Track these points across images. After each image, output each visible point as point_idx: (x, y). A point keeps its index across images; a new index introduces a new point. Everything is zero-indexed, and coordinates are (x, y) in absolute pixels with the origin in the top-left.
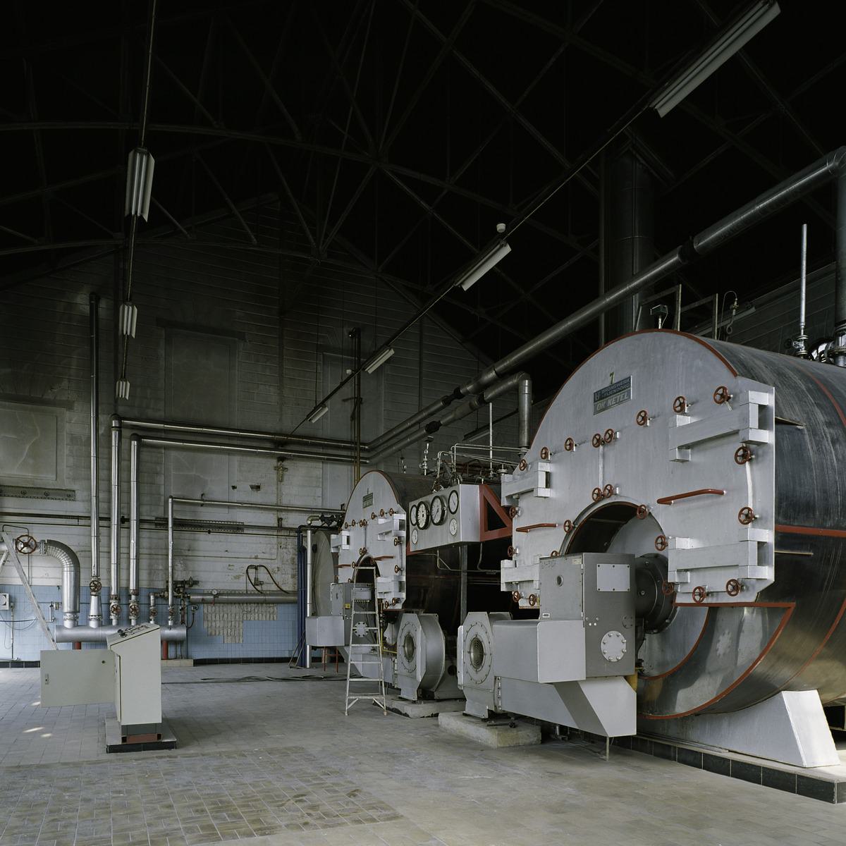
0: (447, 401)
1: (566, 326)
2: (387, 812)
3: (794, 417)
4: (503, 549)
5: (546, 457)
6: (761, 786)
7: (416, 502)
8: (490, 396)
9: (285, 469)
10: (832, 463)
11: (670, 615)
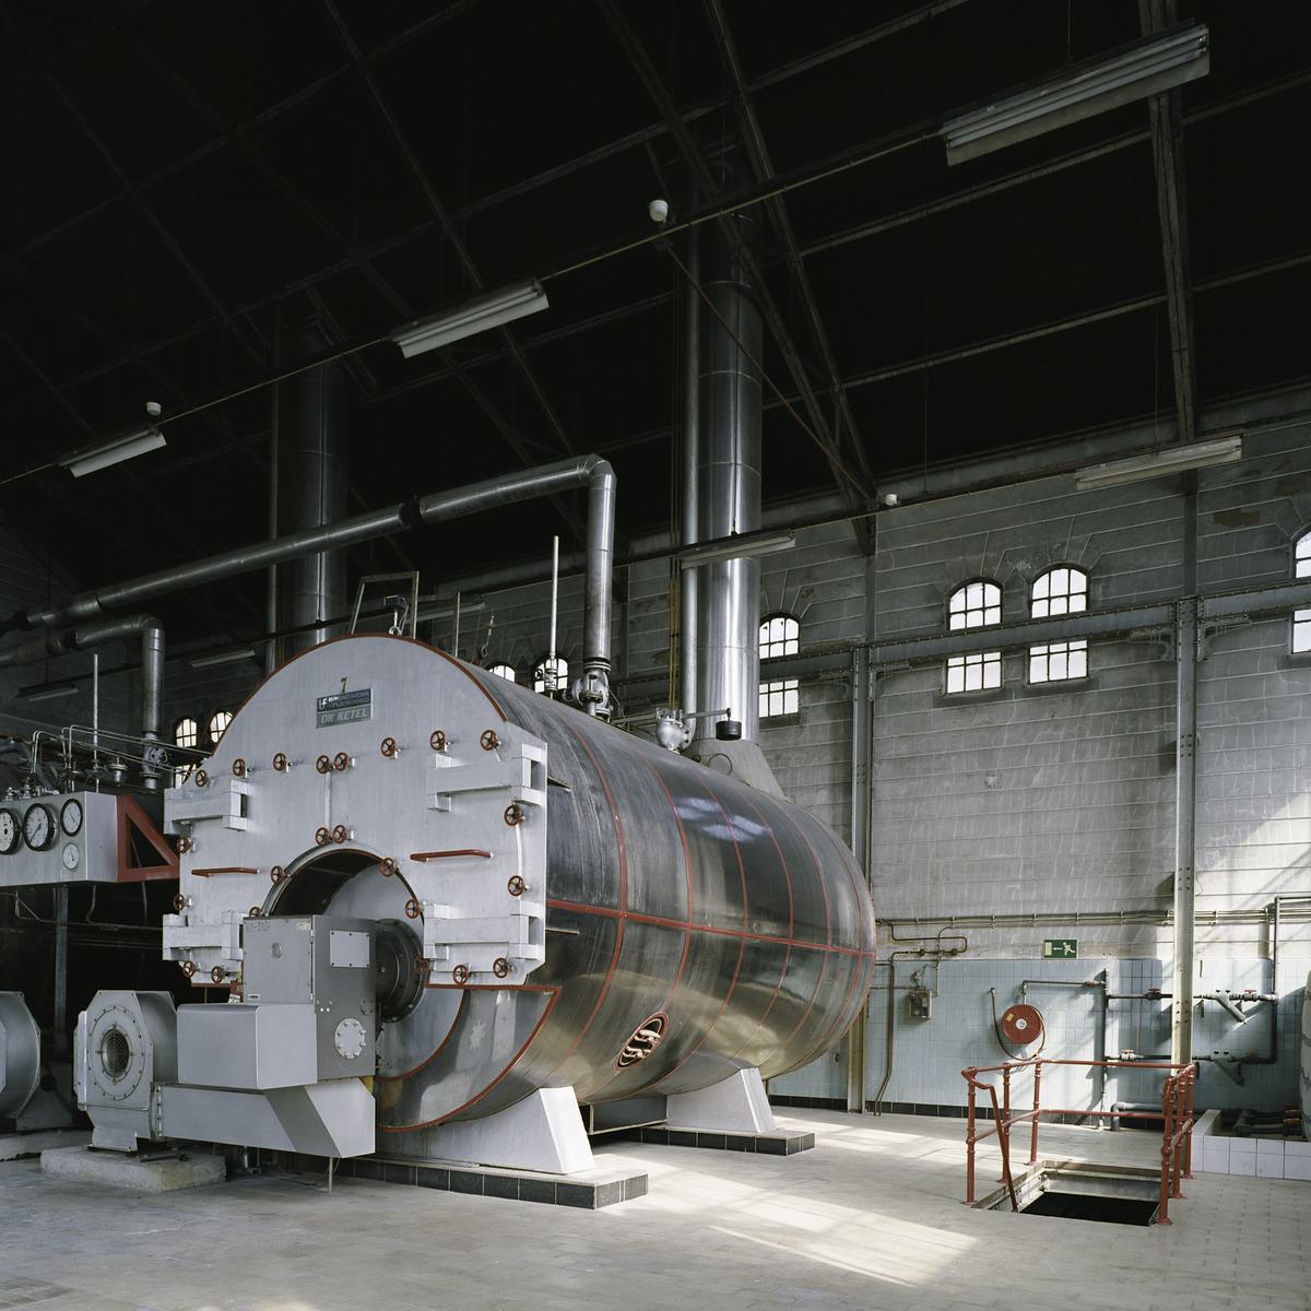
3: (562, 778)
4: (167, 897)
8: (87, 638)
10: (597, 835)
11: (414, 998)
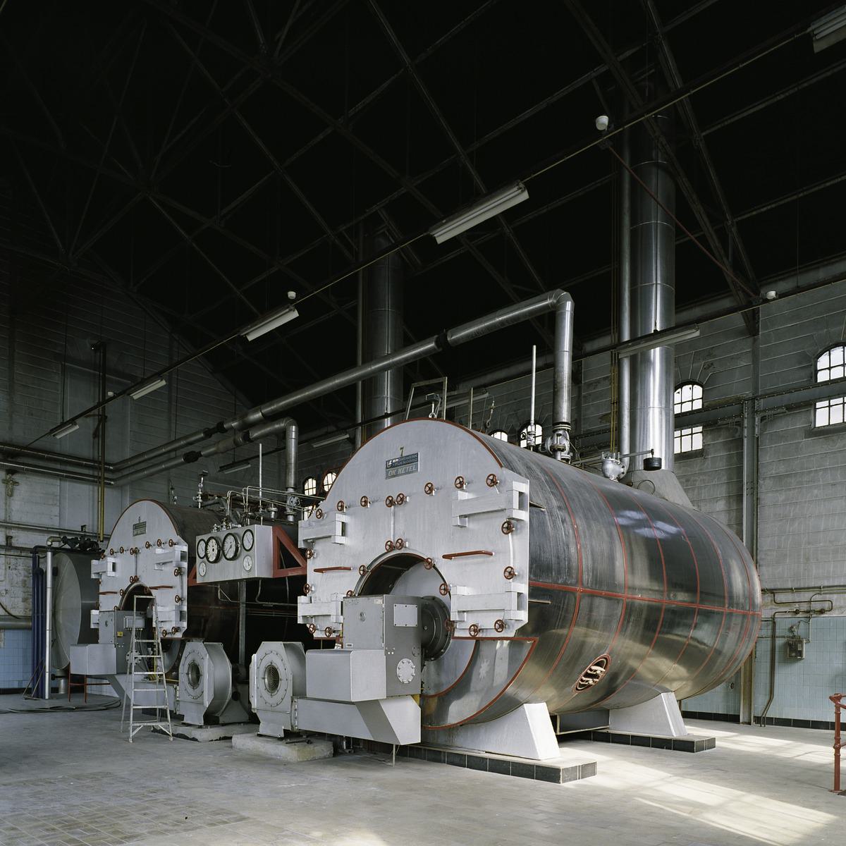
0: (208, 433)
1: (334, 383)
2: (235, 816)
3: (539, 502)
4: (300, 586)
5: (342, 510)
6: (510, 776)
7: (206, 537)
8: (256, 435)
9: (16, 483)
10: (562, 537)
11: (444, 646)
